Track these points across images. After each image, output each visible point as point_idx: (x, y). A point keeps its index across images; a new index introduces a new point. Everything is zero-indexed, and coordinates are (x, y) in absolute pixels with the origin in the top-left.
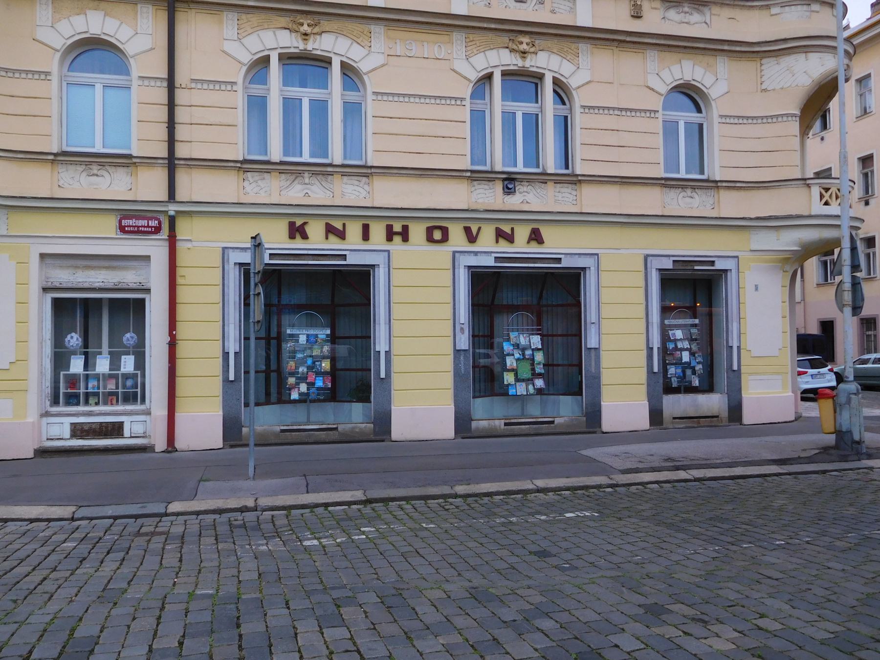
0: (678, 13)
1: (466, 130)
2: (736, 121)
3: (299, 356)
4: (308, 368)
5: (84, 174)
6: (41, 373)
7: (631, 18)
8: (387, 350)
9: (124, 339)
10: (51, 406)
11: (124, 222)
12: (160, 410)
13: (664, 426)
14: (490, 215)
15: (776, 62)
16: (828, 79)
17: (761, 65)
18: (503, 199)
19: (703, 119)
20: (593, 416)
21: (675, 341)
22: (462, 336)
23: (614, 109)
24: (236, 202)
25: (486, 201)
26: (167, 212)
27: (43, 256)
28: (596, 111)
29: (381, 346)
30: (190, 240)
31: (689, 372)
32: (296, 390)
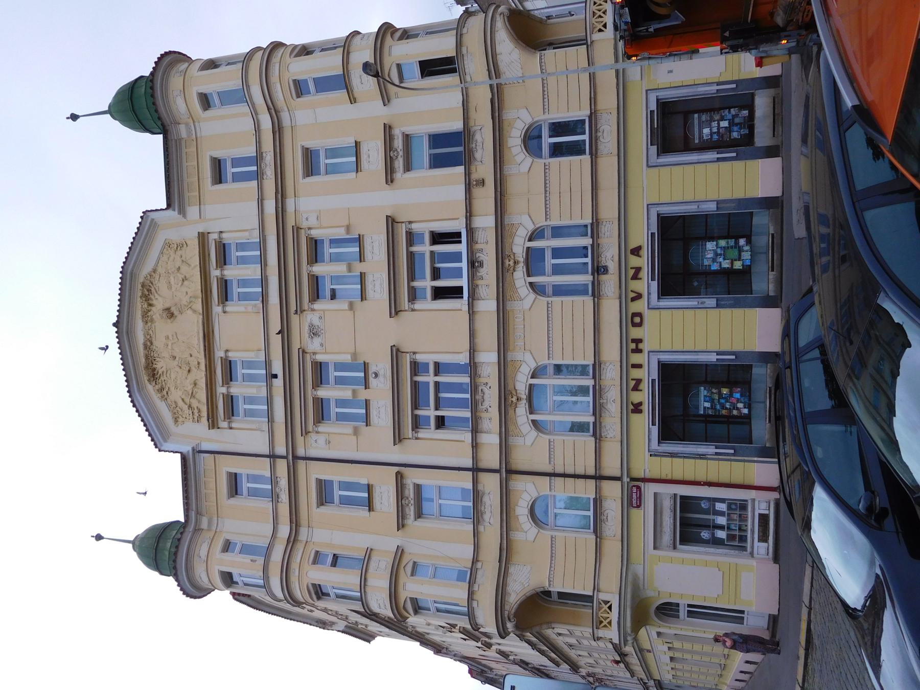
1: (568, 299)
2: (546, 100)
3: (718, 407)
4: (727, 401)
5: (606, 523)
6: (726, 554)
7: (484, 186)
8: (715, 354)
9: (705, 507)
10: (746, 551)
12: (752, 494)
13: (780, 144)
14: (622, 285)
15: (503, 75)
16: (513, 33)
17: (505, 84)
18: (611, 274)
19: (546, 123)
20: (769, 203)
21: (712, 134)
22: (707, 303)
23: (546, 197)
24: (621, 543)
25: (613, 286)
27: (655, 548)
28: (548, 210)
29: (713, 358)
30: (644, 470)
31: (737, 120)
32: (741, 410)
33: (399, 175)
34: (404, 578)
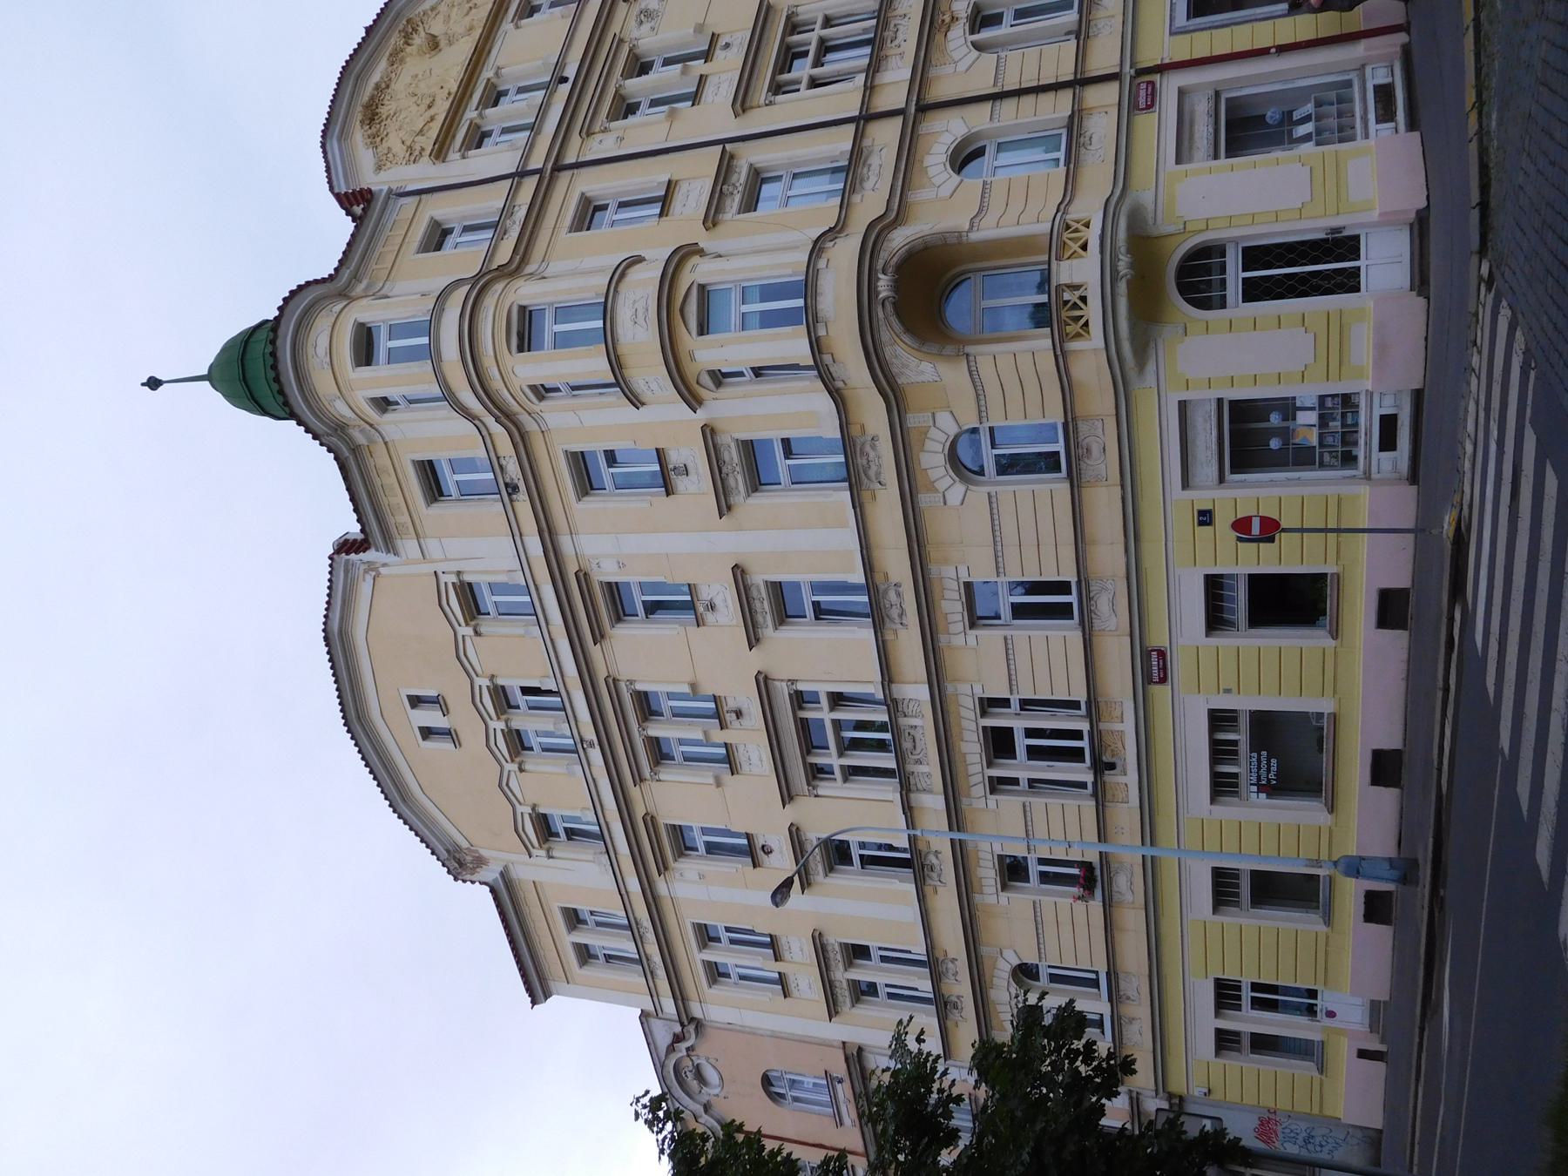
0: (868, 178)
1: (1055, 803)
11: (1142, 105)
26: (1131, 76)
33: (739, 497)
34: (689, 340)
